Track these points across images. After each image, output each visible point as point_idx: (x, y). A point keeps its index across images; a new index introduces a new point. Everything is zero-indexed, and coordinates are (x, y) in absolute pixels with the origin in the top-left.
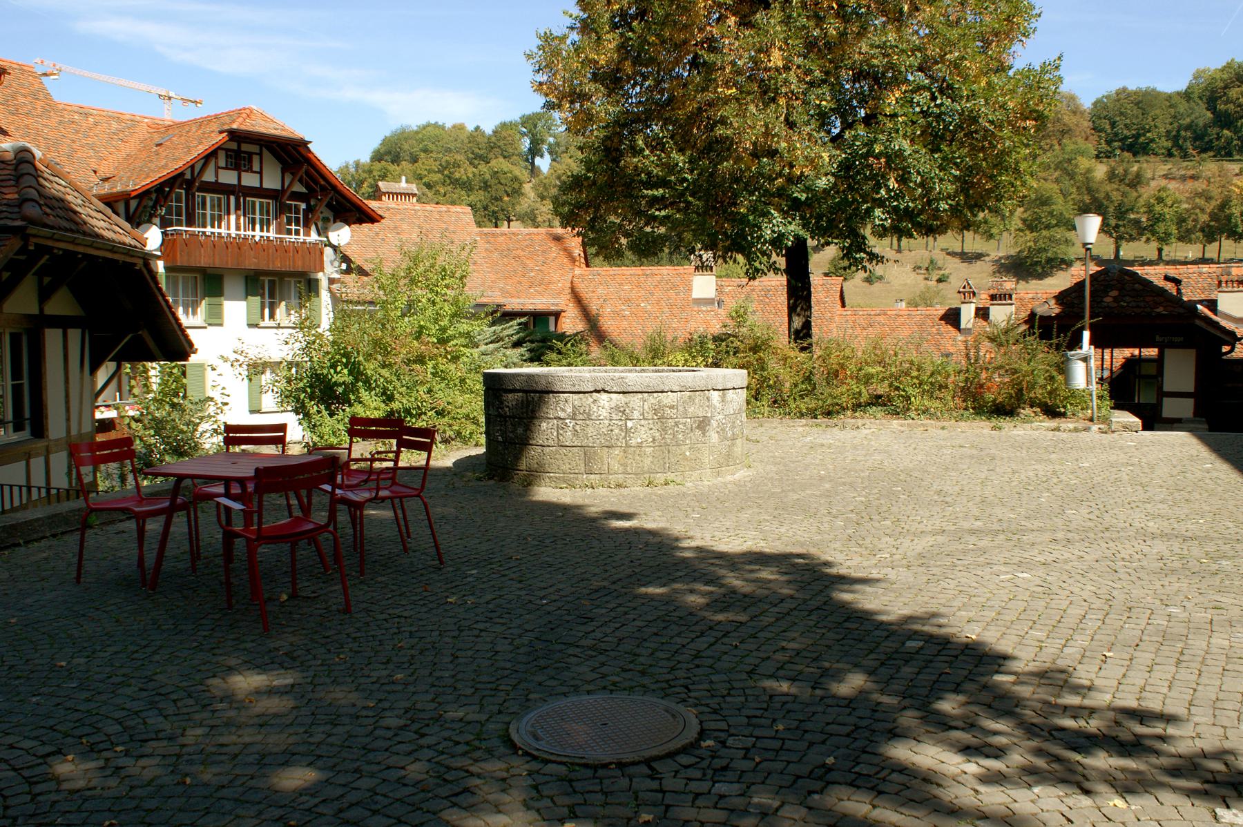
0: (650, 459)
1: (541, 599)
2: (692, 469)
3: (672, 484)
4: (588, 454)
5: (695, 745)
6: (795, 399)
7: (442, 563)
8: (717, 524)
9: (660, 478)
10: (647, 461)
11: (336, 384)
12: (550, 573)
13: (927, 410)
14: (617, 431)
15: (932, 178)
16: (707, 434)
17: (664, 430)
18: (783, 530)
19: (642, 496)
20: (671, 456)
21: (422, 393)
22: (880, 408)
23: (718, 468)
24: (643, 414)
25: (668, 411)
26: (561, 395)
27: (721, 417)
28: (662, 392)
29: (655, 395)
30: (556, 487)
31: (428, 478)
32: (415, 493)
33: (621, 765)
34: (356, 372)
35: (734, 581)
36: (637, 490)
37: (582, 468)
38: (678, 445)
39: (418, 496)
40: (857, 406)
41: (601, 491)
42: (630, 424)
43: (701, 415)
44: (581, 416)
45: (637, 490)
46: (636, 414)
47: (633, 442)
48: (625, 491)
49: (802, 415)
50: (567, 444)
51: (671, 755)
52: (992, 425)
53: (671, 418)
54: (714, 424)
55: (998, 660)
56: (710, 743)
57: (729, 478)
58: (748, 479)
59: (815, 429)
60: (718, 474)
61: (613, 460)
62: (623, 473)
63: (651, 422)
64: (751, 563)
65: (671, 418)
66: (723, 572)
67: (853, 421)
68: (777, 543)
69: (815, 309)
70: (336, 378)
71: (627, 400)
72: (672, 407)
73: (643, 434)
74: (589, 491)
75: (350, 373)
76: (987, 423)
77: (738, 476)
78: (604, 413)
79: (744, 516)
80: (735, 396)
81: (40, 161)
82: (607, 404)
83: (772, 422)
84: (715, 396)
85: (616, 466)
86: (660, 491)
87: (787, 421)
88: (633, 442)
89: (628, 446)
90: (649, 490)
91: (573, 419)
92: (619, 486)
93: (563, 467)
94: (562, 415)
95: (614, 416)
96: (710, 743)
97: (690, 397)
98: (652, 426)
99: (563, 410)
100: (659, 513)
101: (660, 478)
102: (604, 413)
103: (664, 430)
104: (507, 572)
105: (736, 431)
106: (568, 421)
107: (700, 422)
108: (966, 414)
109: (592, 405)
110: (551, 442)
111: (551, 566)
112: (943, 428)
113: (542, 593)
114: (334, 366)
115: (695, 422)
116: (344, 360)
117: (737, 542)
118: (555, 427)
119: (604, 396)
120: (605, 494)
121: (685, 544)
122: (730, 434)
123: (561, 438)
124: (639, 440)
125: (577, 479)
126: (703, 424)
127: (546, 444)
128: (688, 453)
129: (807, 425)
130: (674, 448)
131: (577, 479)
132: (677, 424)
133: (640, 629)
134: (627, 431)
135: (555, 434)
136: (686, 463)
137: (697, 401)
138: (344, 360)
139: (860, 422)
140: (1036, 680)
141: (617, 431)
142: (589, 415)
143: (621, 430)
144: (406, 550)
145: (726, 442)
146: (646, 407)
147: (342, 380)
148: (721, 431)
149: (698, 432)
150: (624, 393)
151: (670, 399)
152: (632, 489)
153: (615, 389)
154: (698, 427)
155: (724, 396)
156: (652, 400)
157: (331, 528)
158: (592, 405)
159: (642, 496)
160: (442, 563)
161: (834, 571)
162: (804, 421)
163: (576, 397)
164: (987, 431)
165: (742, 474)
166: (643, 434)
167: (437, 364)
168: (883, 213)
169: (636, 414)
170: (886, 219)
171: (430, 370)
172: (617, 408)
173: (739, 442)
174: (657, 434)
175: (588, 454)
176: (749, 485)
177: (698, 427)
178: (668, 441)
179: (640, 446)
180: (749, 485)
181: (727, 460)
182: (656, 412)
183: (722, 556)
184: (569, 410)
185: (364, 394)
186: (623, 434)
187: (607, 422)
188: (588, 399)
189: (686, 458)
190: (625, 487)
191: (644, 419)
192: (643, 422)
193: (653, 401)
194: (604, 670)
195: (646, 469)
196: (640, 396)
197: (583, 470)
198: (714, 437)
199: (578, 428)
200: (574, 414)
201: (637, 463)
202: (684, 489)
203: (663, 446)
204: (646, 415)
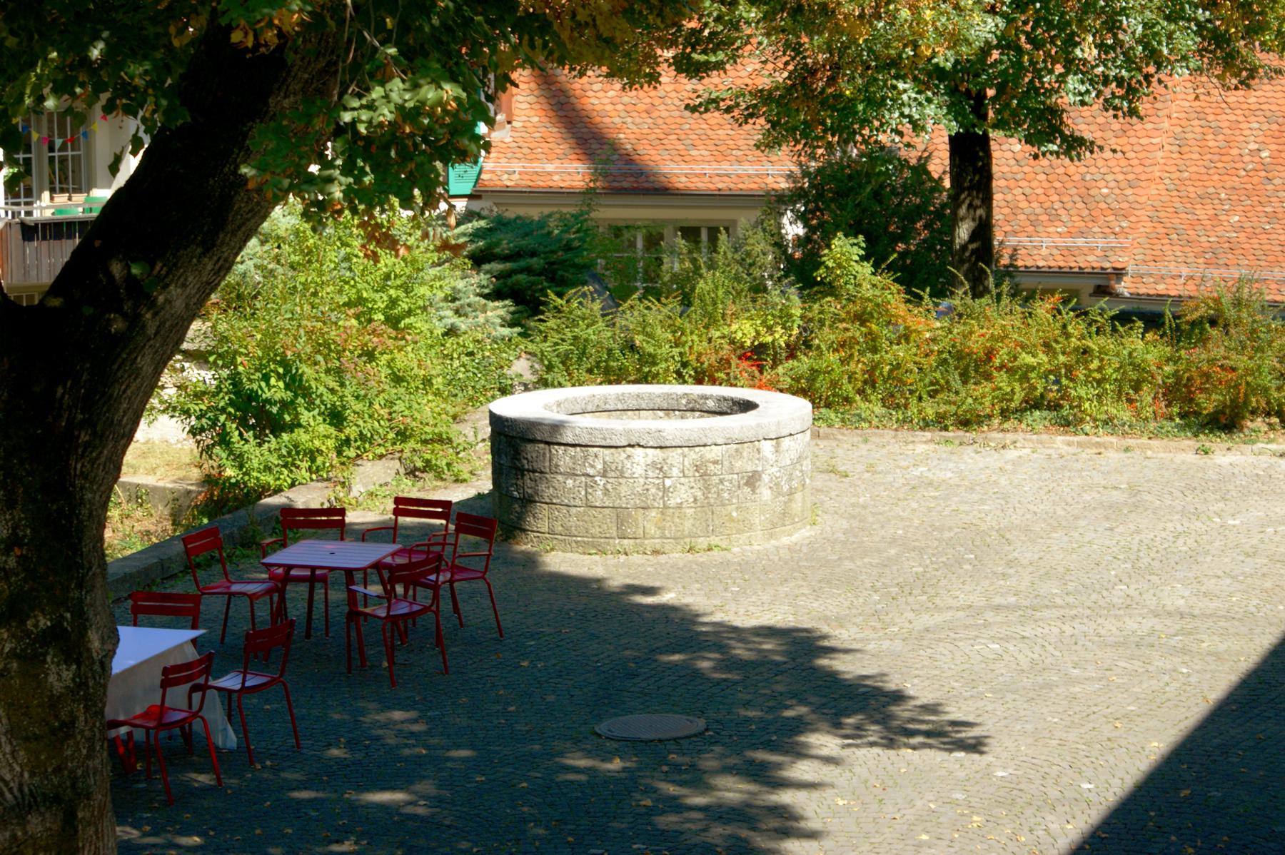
0: (691, 521)
1: (597, 661)
2: (739, 532)
3: (716, 549)
4: (621, 517)
5: (701, 734)
6: (920, 399)
7: (501, 636)
8: (754, 598)
9: (702, 542)
10: (688, 524)
11: (268, 401)
12: (598, 643)
13: (1111, 419)
14: (653, 490)
15: (1156, 34)
16: (757, 491)
17: (707, 488)
18: (816, 605)
19: (681, 565)
20: (715, 517)
21: (377, 407)
22: (1045, 413)
23: (772, 528)
24: (683, 471)
25: (711, 467)
26: (590, 449)
27: (775, 469)
28: (705, 446)
29: (697, 449)
30: (584, 553)
31: (490, 562)
32: (480, 575)
33: (660, 741)
34: (295, 383)
35: (740, 651)
36: (677, 556)
37: (614, 532)
38: (723, 505)
39: (483, 578)
40: (1005, 414)
41: (636, 558)
42: (668, 482)
43: (749, 469)
44: (613, 474)
45: (677, 556)
46: (675, 472)
47: (672, 503)
48: (662, 558)
49: (926, 425)
50: (597, 504)
51: (687, 737)
52: (1199, 445)
53: (715, 474)
54: (766, 478)
55: (898, 697)
56: (711, 733)
57: (785, 540)
58: (807, 542)
59: (942, 448)
60: (771, 536)
61: (649, 523)
62: (661, 537)
63: (692, 479)
64: (759, 635)
65: (715, 474)
66: (733, 643)
67: (1001, 435)
68: (805, 618)
69: (997, 198)
70: (267, 395)
71: (665, 456)
72: (716, 462)
73: (682, 494)
74: (623, 558)
75: (287, 387)
76: (1192, 443)
77: (796, 537)
78: (639, 470)
79: (784, 589)
80: (792, 443)
81: (715, 669)
82: (642, 461)
83: (882, 436)
84: (767, 447)
85: (652, 530)
86: (702, 558)
87: (905, 434)
88: (672, 503)
89: (666, 507)
90: (690, 557)
91: (604, 476)
92: (656, 552)
93: (592, 531)
94: (591, 471)
95: (650, 474)
96: (711, 733)
97: (737, 450)
98: (693, 484)
99: (592, 466)
100: (698, 586)
101: (702, 542)
102: (639, 470)
103: (707, 488)
104: (561, 643)
105: (795, 484)
106: (597, 479)
107: (749, 477)
108: (1168, 425)
109: (626, 461)
110: (578, 502)
111: (598, 638)
112: (1127, 450)
113: (595, 659)
114: (266, 378)
115: (743, 478)
116: (281, 370)
117: (768, 617)
118: (583, 485)
119: (639, 451)
120: (640, 562)
121: (705, 619)
122: (786, 488)
123: (590, 497)
124: (679, 501)
125: (608, 544)
126: (752, 480)
127: (573, 503)
128: (734, 514)
129: (932, 441)
130: (719, 508)
131: (608, 544)
132: (721, 481)
133: (673, 681)
134: (665, 490)
135: (583, 493)
136: (732, 525)
137: (745, 454)
138: (281, 370)
139: (1009, 437)
140: (918, 709)
141: (653, 490)
142: (622, 472)
143: (658, 489)
144: (461, 625)
145: (781, 498)
146: (686, 463)
147: (278, 397)
148: (775, 487)
149: (747, 490)
150: (661, 447)
151: (713, 453)
152: (671, 555)
153: (651, 444)
154: (747, 484)
155: (778, 445)
156: (693, 455)
157: (434, 608)
158: (626, 461)
159: (681, 565)
160: (501, 636)
161: (826, 643)
162: (928, 435)
163: (607, 451)
164: (1191, 457)
165: (803, 534)
166: (682, 494)
167: (393, 360)
168: (1083, 82)
169: (675, 472)
170: (1088, 92)
171: (385, 372)
172: (654, 464)
173: (798, 496)
174: (699, 494)
175: (621, 517)
176: (805, 549)
177: (747, 484)
178: (712, 501)
179: (679, 506)
180: (805, 549)
181: (784, 517)
182: (698, 468)
183: (736, 629)
184: (600, 466)
185: (306, 417)
186: (661, 494)
187: (642, 481)
188: (621, 455)
189: (732, 520)
190: (664, 553)
191: (684, 476)
192: (683, 480)
193: (694, 456)
194: (648, 703)
195: (686, 533)
196: (679, 450)
197: (615, 534)
198: (765, 493)
199: (609, 486)
200: (605, 471)
201: (676, 526)
202: (729, 556)
203: (706, 507)
204: (686, 472)
